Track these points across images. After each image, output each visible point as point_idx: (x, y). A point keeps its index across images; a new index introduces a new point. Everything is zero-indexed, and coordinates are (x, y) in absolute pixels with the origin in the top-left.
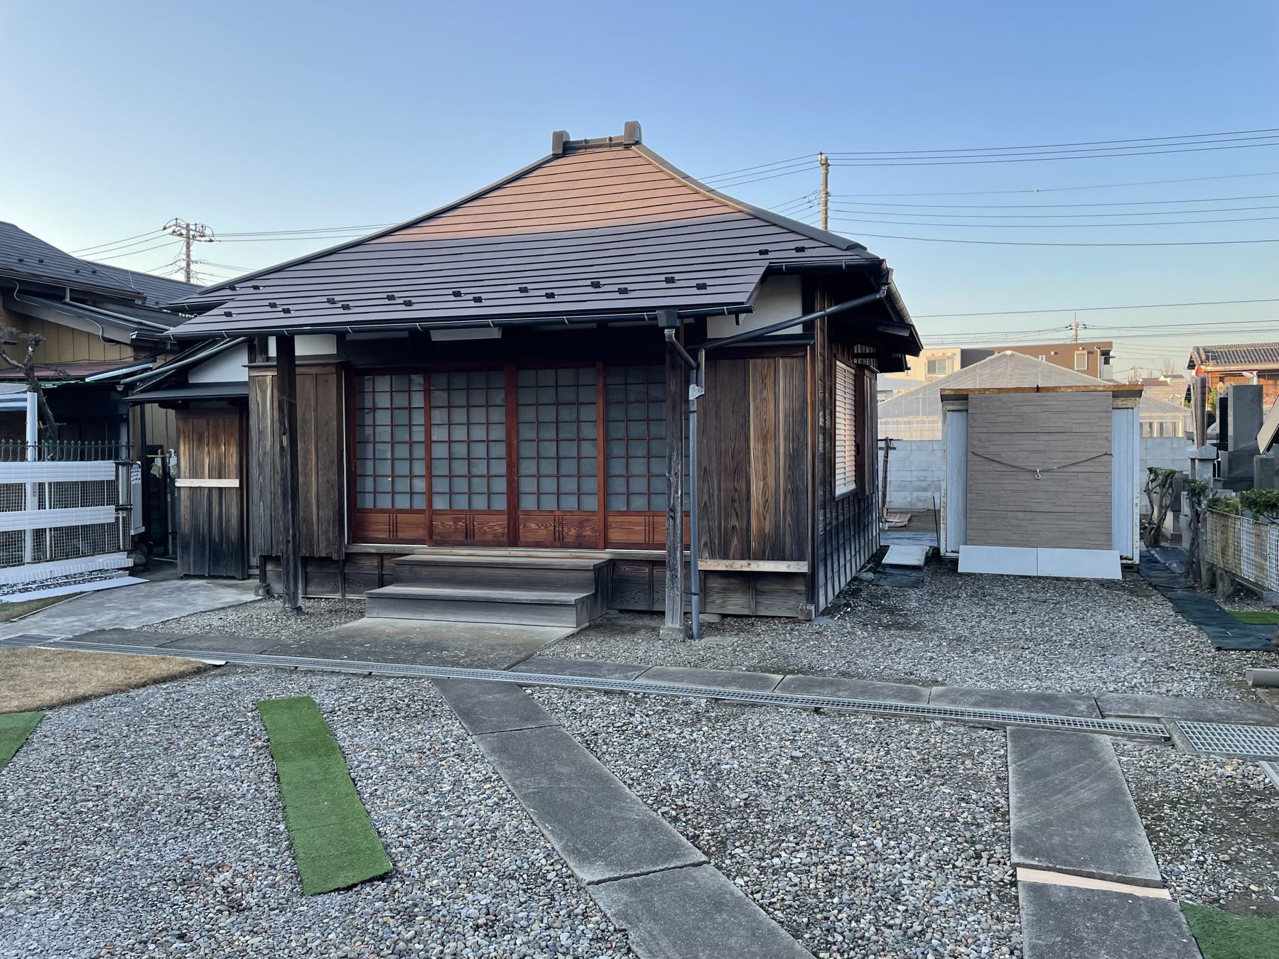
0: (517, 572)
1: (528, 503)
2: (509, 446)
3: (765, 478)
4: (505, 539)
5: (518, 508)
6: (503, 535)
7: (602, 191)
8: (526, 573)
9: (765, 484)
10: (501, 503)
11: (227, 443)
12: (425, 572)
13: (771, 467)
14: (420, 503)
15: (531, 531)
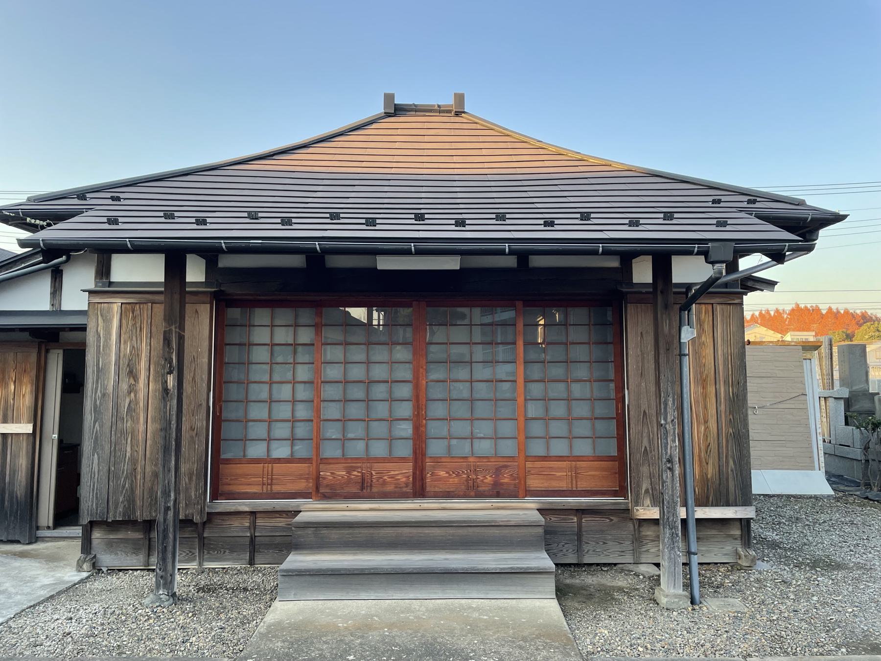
0: (451, 531)
1: (435, 448)
2: (417, 387)
3: (706, 422)
4: (409, 490)
5: (424, 454)
6: (407, 485)
7: (481, 139)
8: (461, 531)
9: (707, 428)
10: (405, 450)
11: (17, 382)
12: (334, 534)
13: (712, 411)
14: (302, 450)
15: (440, 479)
